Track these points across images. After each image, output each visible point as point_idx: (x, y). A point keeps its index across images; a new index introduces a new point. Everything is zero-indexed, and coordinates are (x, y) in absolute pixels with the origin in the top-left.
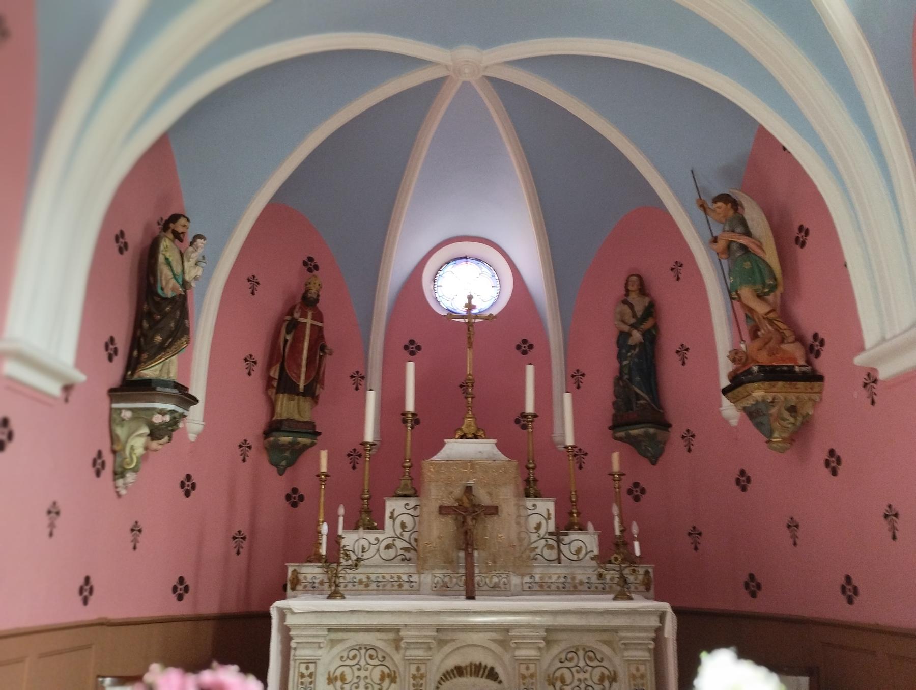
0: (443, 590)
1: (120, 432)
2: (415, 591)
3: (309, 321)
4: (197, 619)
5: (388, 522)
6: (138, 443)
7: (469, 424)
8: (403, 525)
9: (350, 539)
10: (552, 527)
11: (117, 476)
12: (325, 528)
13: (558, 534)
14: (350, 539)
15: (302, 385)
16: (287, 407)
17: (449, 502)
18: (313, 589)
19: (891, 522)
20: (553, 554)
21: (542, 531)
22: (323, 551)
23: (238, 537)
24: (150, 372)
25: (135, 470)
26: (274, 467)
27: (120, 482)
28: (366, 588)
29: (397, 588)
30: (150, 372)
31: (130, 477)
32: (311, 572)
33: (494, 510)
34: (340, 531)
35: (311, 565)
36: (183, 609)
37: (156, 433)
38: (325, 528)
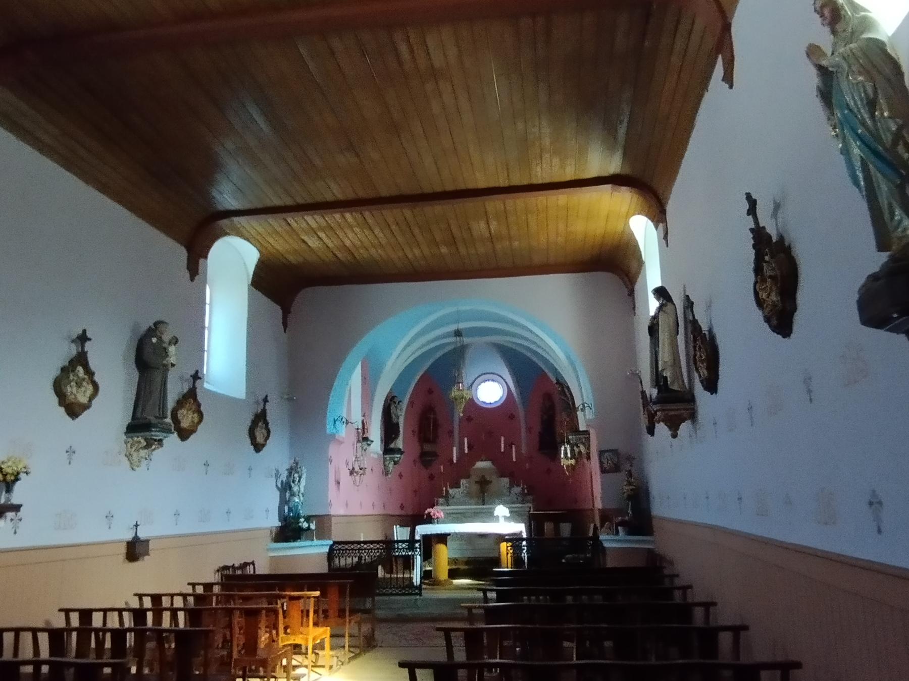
0: (477, 504)
1: (387, 463)
2: (470, 504)
3: (432, 416)
4: (407, 516)
5: (462, 486)
6: (391, 465)
7: (483, 457)
8: (466, 487)
9: (451, 491)
10: (508, 486)
11: (10, 478)
12: (444, 489)
13: (510, 488)
14: (451, 491)
15: (431, 439)
16: (428, 447)
17: (477, 480)
18: (442, 505)
19: (207, 463)
20: (508, 493)
21: (506, 487)
22: (444, 494)
23: (415, 491)
24: (392, 446)
25: (391, 473)
26: (789, 542)
27: (387, 477)
28: (456, 504)
29: (465, 504)
30: (392, 446)
31: (390, 476)
32: (441, 500)
33: (491, 482)
34: (448, 489)
35: (475, 319)
36: (403, 513)
37: (395, 463)
38: (444, 489)
